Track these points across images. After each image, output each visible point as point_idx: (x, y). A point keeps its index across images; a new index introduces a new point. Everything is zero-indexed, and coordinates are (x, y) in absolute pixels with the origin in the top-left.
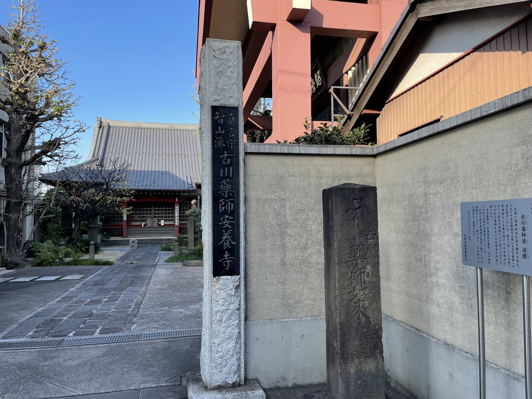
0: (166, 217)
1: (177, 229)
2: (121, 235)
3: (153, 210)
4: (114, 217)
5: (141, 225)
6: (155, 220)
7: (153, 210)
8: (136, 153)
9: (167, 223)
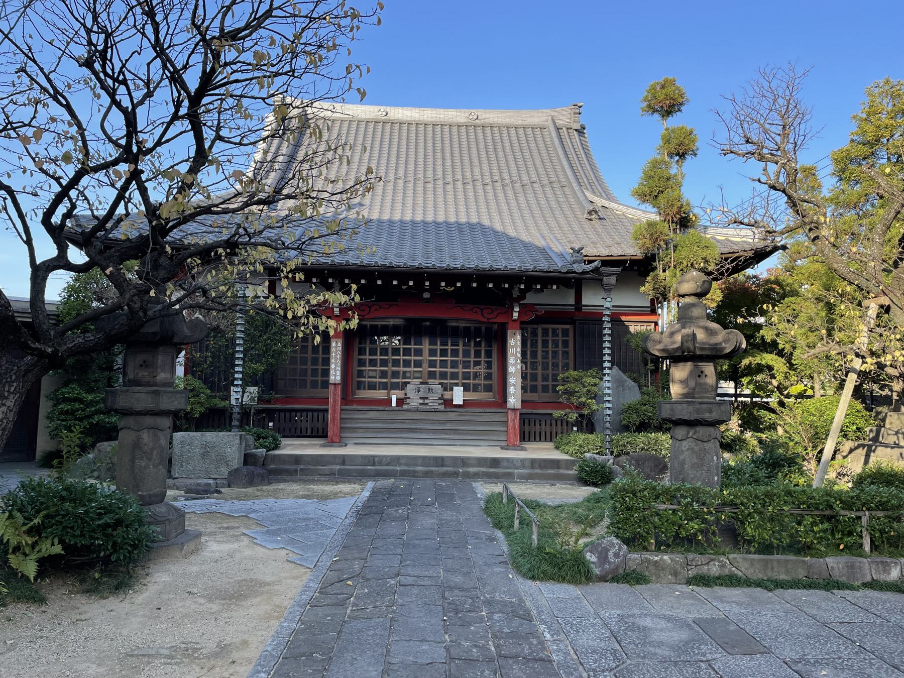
0: (466, 376)
1: (514, 420)
2: (320, 433)
3: (426, 352)
4: (304, 372)
7: (426, 352)
9: (473, 396)
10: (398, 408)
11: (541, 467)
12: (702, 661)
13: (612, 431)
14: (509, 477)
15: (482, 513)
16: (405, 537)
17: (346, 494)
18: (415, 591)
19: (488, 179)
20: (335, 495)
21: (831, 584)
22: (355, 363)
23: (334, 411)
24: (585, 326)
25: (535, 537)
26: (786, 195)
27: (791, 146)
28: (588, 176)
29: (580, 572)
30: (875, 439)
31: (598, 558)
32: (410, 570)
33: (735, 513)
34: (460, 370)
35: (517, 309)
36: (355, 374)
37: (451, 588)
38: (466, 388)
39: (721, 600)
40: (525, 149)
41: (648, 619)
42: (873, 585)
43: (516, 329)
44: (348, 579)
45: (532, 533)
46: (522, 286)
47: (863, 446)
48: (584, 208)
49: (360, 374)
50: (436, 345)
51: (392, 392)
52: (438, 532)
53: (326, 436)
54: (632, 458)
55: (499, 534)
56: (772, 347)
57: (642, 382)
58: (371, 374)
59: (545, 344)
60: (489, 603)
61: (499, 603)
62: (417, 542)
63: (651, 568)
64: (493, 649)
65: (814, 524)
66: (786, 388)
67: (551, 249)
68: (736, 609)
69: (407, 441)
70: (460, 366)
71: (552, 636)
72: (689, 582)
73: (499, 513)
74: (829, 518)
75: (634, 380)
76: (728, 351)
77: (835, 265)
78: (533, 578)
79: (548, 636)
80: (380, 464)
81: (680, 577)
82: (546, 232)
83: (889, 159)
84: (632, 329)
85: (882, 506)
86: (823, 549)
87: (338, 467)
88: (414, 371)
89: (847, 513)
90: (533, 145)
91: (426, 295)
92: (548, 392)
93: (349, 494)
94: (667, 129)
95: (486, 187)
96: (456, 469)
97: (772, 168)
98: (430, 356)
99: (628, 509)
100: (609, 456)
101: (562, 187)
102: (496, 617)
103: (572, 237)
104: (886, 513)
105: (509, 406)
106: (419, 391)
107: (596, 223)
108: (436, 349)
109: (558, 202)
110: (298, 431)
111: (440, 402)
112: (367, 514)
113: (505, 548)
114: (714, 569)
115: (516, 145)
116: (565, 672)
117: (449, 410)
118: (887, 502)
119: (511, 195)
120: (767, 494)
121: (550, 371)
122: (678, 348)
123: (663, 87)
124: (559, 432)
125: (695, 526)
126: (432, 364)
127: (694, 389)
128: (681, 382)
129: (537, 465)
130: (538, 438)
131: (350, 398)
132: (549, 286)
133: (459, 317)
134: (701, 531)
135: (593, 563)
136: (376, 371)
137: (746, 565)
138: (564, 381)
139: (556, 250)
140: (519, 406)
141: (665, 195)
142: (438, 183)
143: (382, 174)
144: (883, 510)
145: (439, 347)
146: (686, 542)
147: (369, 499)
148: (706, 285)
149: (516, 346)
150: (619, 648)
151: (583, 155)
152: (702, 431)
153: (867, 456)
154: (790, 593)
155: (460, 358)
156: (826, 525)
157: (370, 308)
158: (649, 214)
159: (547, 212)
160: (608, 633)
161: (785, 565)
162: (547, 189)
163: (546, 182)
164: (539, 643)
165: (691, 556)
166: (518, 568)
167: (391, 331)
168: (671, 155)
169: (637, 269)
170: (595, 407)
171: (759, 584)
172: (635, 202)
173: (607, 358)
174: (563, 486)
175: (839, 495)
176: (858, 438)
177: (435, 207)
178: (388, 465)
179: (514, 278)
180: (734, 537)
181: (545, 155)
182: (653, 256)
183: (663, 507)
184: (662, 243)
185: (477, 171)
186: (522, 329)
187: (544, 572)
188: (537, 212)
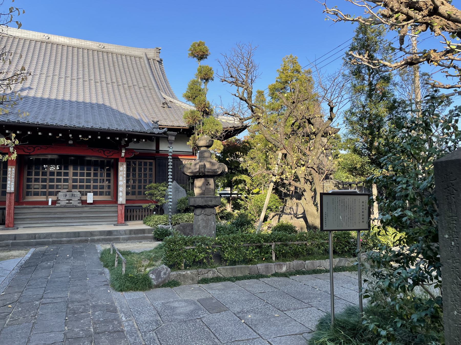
0: (95, 187)
1: (121, 210)
5: (47, 202)
6: (76, 192)
8: (41, 74)
9: (99, 198)
10: (53, 206)
11: (135, 234)
12: (198, 319)
13: (172, 213)
14: (117, 240)
15: (99, 260)
16: (49, 278)
17: (15, 257)
18: (51, 306)
19: (109, 81)
20: (8, 258)
21: (259, 276)
22: (25, 181)
23: (10, 209)
24: (160, 160)
25: (124, 269)
26: (247, 103)
27: (250, 81)
28: (162, 84)
29: (146, 284)
30: (282, 211)
31: (156, 276)
32: (49, 296)
33: (220, 248)
34: (92, 184)
35: (124, 151)
36: (25, 187)
37: (72, 302)
38: (95, 194)
39: (212, 289)
40: (131, 67)
41: (176, 303)
42: (276, 275)
43: (123, 162)
44: (9, 304)
45: (122, 267)
46: (126, 139)
47: (278, 214)
48: (160, 101)
49: (28, 187)
50: (77, 170)
51: (49, 197)
52: (70, 272)
53: (4, 224)
54: (181, 226)
55: (107, 270)
56: (245, 172)
57: (187, 188)
58: (35, 187)
59: (140, 170)
60: (94, 307)
61: (100, 306)
62: (56, 279)
63: (182, 278)
64: (92, 330)
65: (253, 250)
66: (251, 190)
67: (142, 120)
68: (217, 292)
70: (92, 182)
71: (126, 318)
72: (199, 283)
73: (107, 260)
74: (260, 247)
75: (183, 187)
76: (219, 173)
77: (266, 135)
78: (121, 291)
79: (124, 319)
80: (39, 238)
81: (195, 280)
82: (140, 112)
83: (291, 90)
84: (183, 162)
85: (280, 240)
86: (256, 261)
87: (11, 241)
88: (63, 185)
89: (266, 244)
90: (135, 66)
91: (71, 142)
92: (141, 195)
93: (17, 256)
94: (200, 66)
95: (108, 85)
96: (86, 238)
97: (241, 90)
98: (73, 176)
99: (172, 250)
100: (170, 225)
101: (150, 89)
102: (97, 313)
103: (154, 115)
104: (281, 243)
105: (119, 202)
106: (66, 196)
107: (167, 109)
108: (84, 173)
109: (148, 97)
111: (79, 201)
112: (27, 267)
113: (108, 277)
114: (210, 275)
115: (126, 65)
116: (130, 335)
117: (85, 206)
118: (282, 238)
119: (122, 91)
120: (234, 238)
121: (142, 184)
122: (197, 172)
123: (199, 45)
124: (146, 215)
125: (202, 255)
126: (75, 181)
127: (204, 191)
128: (199, 187)
129: (133, 233)
130: (135, 219)
132: (141, 140)
133: (92, 155)
134: (205, 258)
135: (153, 279)
136: (39, 185)
137: (224, 271)
138: (149, 189)
139: (146, 122)
140: (124, 202)
141: (198, 98)
142: (61, 79)
143: (32, 71)
144: (281, 241)
145: (85, 172)
146: (199, 264)
147: (30, 258)
148: (211, 142)
150: (160, 319)
151: (161, 74)
152: (208, 210)
153: (279, 219)
154: (246, 282)
155: (92, 177)
156: (258, 250)
157: (34, 148)
158: (190, 107)
159: (141, 101)
160: (155, 312)
161: (241, 269)
162: (142, 89)
163: (141, 86)
164: (118, 323)
165: (200, 270)
166: (113, 287)
167: (52, 162)
168: (202, 79)
169: (185, 134)
170: (164, 201)
171: (229, 279)
172: (185, 100)
173: (170, 177)
174: (146, 242)
175: (263, 237)
176: (276, 211)
177: (77, 93)
178: (44, 238)
179: (122, 134)
180: (220, 259)
181: (141, 72)
182: (193, 127)
183: (188, 248)
184: (197, 121)
185: (103, 76)
186: (127, 162)
187: (127, 287)
188: (136, 101)
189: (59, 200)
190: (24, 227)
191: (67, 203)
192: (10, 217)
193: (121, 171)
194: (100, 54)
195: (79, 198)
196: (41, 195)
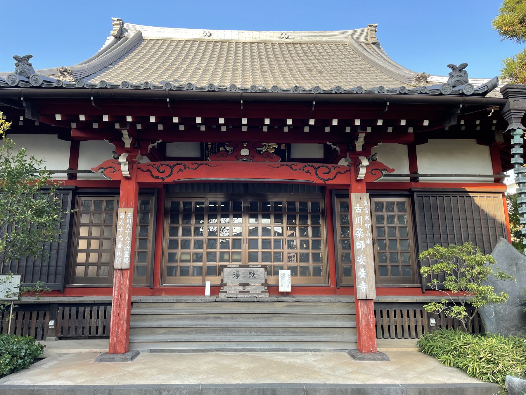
5: (202, 290)
9: (302, 281)
10: (213, 298)
22: (166, 245)
23: (119, 308)
51: (208, 277)
69: (222, 346)
88: (233, 253)
92: (387, 274)
105: (361, 295)
106: (238, 276)
110: (93, 330)
111: (263, 288)
117: (275, 299)
131: (158, 286)
140: (372, 295)
149: (363, 214)
157: (172, 168)
189: (225, 285)
190: (152, 351)
191: (240, 292)
192: (119, 327)
193: (358, 215)
194: (284, 46)
195: (263, 282)
196: (193, 274)
